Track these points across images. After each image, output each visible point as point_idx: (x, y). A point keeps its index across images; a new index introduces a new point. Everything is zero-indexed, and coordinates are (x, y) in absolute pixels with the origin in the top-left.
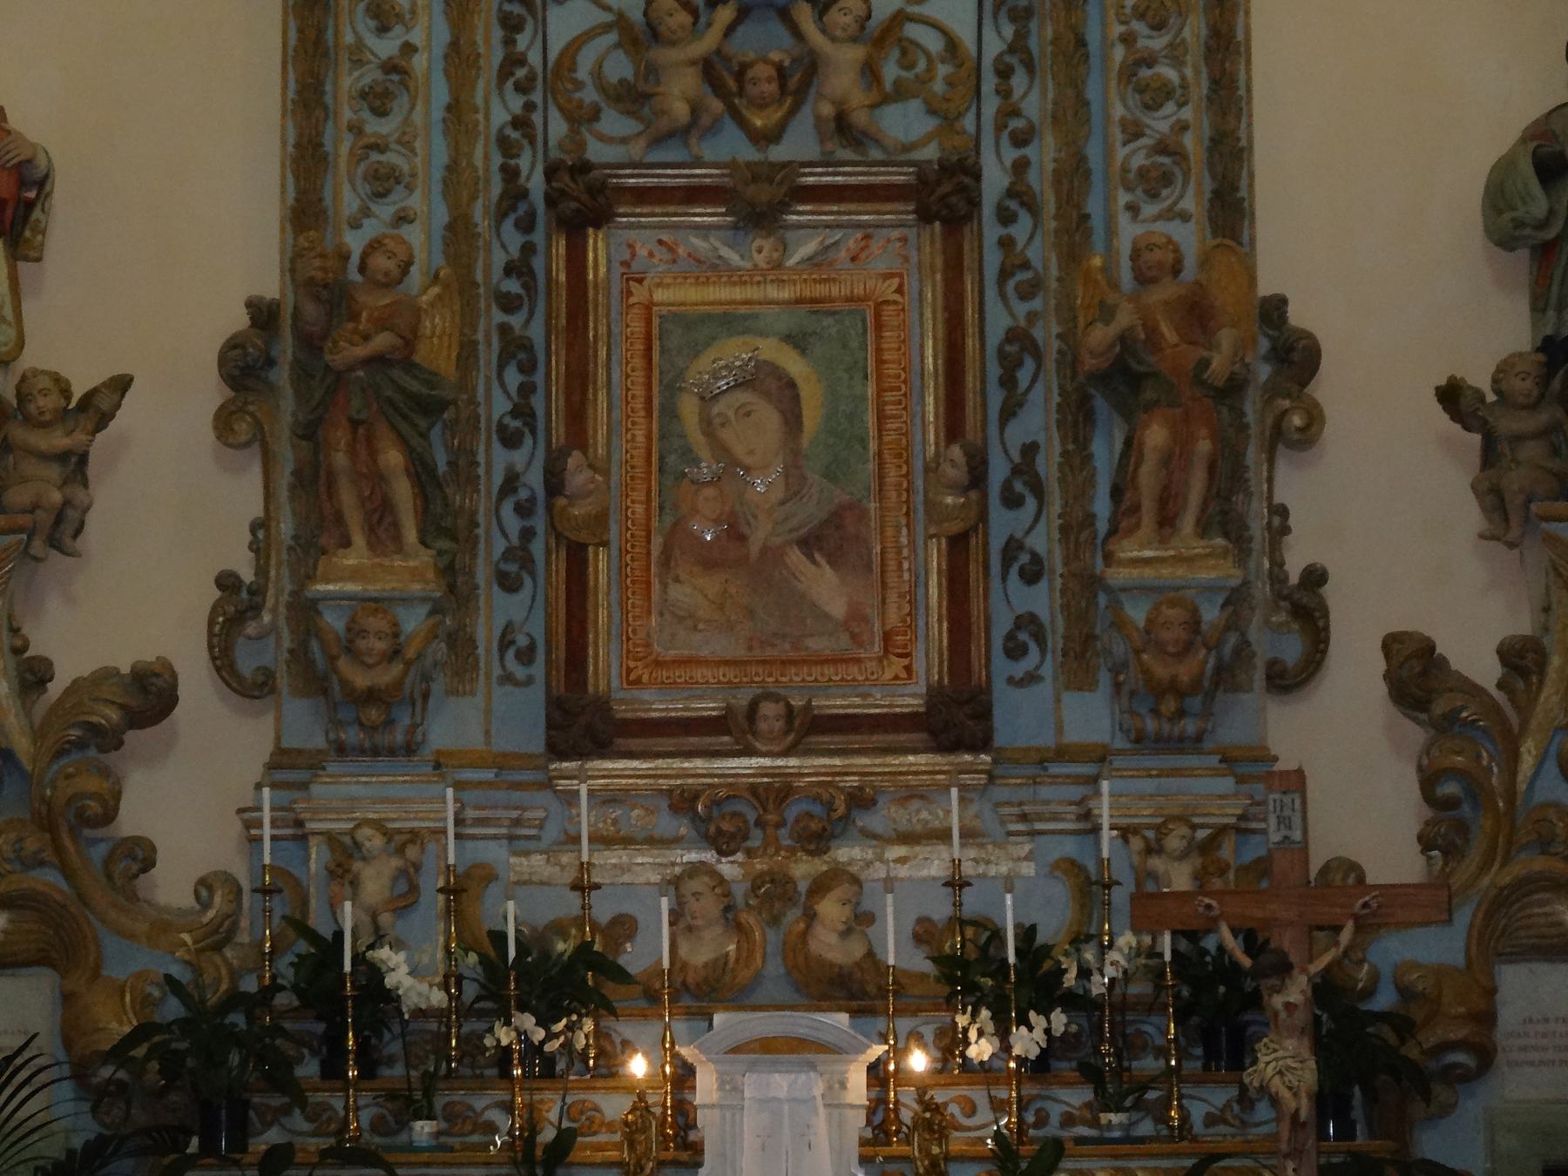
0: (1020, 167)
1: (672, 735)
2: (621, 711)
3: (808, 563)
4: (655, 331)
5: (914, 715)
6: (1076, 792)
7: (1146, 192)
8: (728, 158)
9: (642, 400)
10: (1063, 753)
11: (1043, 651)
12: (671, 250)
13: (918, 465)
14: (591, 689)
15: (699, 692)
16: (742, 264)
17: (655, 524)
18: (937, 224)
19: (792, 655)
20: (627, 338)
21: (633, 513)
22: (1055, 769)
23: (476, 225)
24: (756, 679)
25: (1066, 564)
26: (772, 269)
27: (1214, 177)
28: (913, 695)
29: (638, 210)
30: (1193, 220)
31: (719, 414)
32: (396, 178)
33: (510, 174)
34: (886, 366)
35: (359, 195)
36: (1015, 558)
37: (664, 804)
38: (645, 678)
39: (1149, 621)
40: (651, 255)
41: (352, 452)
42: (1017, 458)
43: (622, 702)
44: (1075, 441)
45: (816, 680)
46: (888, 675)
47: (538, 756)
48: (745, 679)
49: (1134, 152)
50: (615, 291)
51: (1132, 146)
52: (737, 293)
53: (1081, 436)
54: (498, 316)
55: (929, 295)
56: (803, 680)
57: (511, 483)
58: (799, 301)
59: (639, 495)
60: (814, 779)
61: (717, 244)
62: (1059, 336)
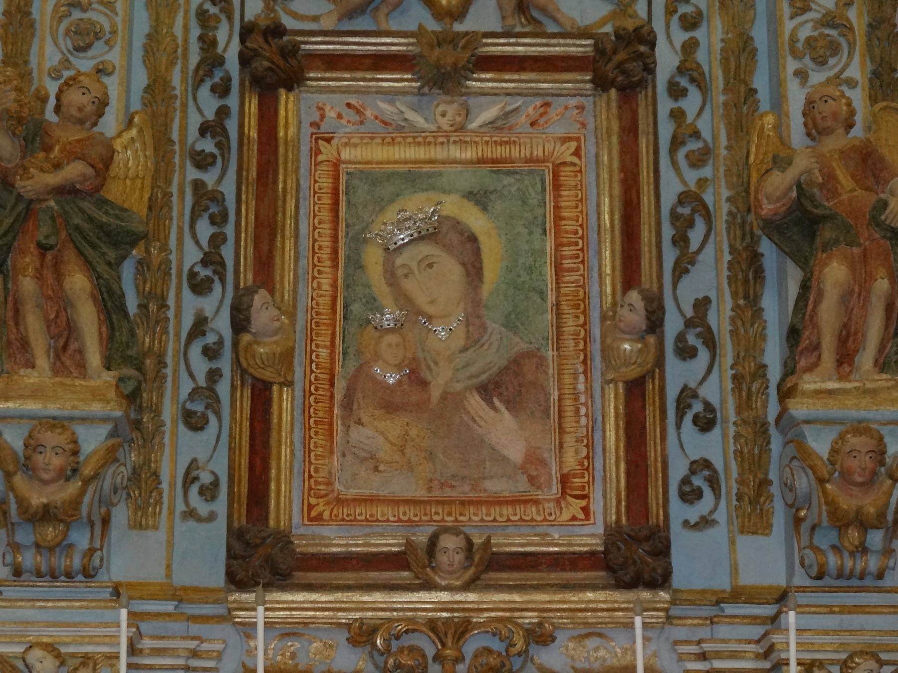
0: (690, 47)
1: (354, 569)
2: (301, 546)
3: (487, 409)
4: (342, 187)
5: (592, 554)
6: (758, 631)
7: (813, 59)
8: (413, 28)
9: (328, 250)
10: (738, 595)
11: (718, 496)
12: (358, 112)
13: (595, 316)
14: (272, 523)
15: (379, 530)
16: (426, 126)
17: (338, 369)
18: (613, 91)
19: (472, 495)
20: (315, 193)
21: (317, 356)
22: (730, 609)
23: (174, 88)
24: (435, 518)
25: (738, 413)
26: (455, 131)
27: (872, 60)
28: (592, 536)
29: (328, 75)
30: (859, 87)
31: (404, 265)
32: (96, 34)
33: (208, 43)
34: (564, 222)
35: (59, 48)
36: (690, 406)
37: (342, 637)
38: (326, 515)
39: (834, 451)
40: (340, 116)
41: (39, 277)
42: (689, 313)
43: (302, 537)
44: (746, 297)
45: (495, 520)
46: (566, 516)
47: (219, 590)
48: (424, 518)
49: (802, 24)
50: (305, 149)
51: (799, 19)
52: (421, 153)
53: (751, 292)
54: (192, 173)
55: (606, 158)
56: (482, 520)
57: (200, 326)
58: (481, 161)
59: (325, 340)
60: (493, 614)
61: (403, 108)
62: (729, 200)
